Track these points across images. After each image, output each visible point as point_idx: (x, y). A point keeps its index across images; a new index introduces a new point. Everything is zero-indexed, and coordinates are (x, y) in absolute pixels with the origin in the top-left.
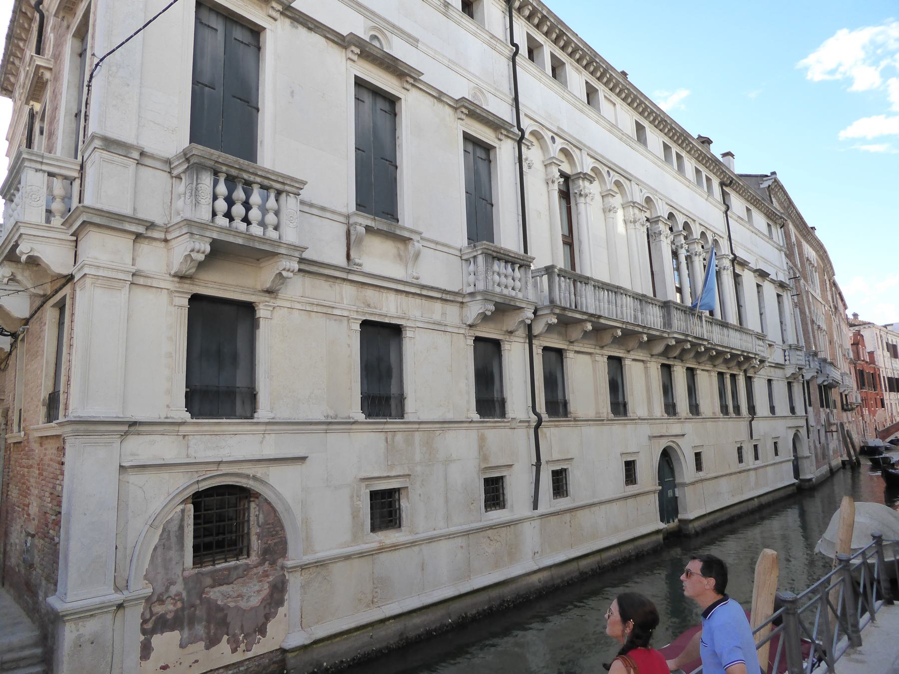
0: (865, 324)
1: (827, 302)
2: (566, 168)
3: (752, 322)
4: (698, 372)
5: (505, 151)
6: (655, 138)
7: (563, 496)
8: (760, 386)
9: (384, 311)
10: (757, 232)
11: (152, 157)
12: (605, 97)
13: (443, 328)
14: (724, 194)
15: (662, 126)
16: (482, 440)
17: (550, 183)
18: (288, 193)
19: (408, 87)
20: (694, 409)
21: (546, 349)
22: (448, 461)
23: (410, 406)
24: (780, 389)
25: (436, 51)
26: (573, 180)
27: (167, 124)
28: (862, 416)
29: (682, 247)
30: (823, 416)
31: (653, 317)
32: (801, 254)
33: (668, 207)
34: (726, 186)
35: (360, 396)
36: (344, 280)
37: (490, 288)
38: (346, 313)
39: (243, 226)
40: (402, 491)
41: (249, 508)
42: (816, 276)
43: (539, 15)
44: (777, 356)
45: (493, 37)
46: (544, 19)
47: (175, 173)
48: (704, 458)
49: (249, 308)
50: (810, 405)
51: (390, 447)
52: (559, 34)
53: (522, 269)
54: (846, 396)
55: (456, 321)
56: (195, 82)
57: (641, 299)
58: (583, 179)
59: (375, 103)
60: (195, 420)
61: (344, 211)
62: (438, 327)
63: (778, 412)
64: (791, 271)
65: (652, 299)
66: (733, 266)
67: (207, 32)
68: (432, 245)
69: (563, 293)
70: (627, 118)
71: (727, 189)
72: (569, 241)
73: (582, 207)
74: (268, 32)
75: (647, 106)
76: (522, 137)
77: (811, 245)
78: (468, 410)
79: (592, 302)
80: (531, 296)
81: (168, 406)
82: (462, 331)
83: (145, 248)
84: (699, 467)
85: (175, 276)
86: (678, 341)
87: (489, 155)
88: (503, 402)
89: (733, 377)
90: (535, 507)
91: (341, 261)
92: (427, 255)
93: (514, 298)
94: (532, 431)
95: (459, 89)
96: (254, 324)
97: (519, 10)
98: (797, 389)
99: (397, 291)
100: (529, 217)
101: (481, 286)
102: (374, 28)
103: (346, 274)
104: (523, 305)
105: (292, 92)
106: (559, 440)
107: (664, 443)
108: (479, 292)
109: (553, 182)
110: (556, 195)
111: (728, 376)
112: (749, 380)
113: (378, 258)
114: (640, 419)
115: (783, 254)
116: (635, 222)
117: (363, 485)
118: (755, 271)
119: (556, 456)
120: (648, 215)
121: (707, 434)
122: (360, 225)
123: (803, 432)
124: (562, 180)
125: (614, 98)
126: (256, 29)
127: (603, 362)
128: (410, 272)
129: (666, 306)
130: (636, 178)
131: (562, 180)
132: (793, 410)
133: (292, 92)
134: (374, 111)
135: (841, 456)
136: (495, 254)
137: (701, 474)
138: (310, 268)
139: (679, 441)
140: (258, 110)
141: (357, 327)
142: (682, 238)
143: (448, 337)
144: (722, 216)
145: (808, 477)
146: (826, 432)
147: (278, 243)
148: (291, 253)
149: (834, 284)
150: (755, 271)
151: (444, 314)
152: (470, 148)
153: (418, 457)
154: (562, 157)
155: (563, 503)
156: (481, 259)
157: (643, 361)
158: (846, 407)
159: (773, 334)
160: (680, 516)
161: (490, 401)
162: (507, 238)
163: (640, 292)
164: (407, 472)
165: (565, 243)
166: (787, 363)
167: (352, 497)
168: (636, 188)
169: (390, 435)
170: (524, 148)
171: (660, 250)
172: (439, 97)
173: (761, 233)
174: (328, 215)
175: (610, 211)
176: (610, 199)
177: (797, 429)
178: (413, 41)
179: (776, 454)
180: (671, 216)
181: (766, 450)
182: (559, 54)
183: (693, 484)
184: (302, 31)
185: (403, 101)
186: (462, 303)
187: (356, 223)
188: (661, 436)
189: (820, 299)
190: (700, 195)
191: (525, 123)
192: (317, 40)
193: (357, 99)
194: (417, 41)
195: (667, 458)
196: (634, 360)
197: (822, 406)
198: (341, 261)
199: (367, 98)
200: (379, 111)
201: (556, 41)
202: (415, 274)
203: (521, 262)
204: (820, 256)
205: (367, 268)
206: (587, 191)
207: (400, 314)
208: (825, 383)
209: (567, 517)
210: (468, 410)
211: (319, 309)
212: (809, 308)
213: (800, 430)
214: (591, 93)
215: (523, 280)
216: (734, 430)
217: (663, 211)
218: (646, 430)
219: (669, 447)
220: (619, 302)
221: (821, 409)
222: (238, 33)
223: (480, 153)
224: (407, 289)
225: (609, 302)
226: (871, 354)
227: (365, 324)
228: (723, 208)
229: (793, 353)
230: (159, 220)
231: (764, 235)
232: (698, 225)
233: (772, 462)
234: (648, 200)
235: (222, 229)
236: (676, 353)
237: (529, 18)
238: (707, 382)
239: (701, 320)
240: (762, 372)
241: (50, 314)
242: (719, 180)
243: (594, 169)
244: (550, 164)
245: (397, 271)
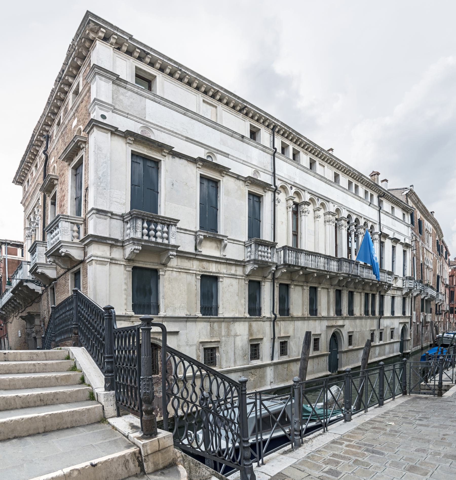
2: (297, 200)
3: (387, 267)
5: (268, 197)
6: (344, 180)
7: (284, 355)
8: (387, 300)
9: (210, 270)
11: (116, 215)
12: (320, 164)
13: (235, 277)
14: (380, 202)
15: (348, 173)
16: (250, 326)
17: (288, 208)
18: (172, 225)
19: (224, 175)
20: (351, 312)
21: (281, 284)
22: (236, 335)
23: (220, 311)
24: (398, 301)
25: (237, 158)
26: (300, 206)
27: (121, 202)
28: (449, 319)
29: (353, 231)
30: (422, 317)
31: (334, 266)
34: (381, 197)
35: (200, 306)
36: (194, 258)
37: (257, 258)
38: (195, 272)
39: (153, 239)
40: (217, 349)
41: (157, 353)
42: (431, 238)
44: (399, 284)
45: (264, 147)
47: (125, 220)
48: (353, 338)
49: (156, 271)
50: (414, 311)
51: (212, 328)
52: (298, 139)
53: (272, 249)
55: (241, 273)
56: (132, 185)
57: (328, 258)
58: (305, 204)
59: (209, 184)
60: (136, 315)
61: (194, 230)
62: (233, 276)
63: (396, 315)
64: (414, 237)
65: (335, 258)
66: (380, 238)
67: (136, 165)
68: (232, 242)
69: (291, 258)
70: (328, 172)
71: (382, 199)
72: (296, 234)
73: (303, 217)
74: (162, 162)
75: (341, 165)
76: (276, 189)
78: (245, 313)
79: (303, 261)
80: (275, 260)
81: (126, 310)
82: (244, 278)
83: (115, 249)
84: (350, 343)
85: (126, 259)
86: (344, 278)
87: (260, 200)
88: (260, 309)
89: (374, 296)
90: (272, 359)
91: (193, 251)
92: (229, 246)
93: (267, 262)
94: (272, 323)
95: (247, 172)
96: (157, 277)
97: (278, 132)
98: (408, 301)
99: (97, 257)
100: (277, 224)
101: (253, 257)
102: (208, 153)
103: (194, 256)
104: (271, 265)
105: (173, 184)
106: (284, 328)
107: (333, 330)
108: (252, 260)
109: (290, 208)
110: (290, 213)
111: (370, 295)
112: (382, 297)
113: (209, 249)
114: (323, 317)
115: (410, 229)
116: (329, 221)
117: (201, 345)
118: (392, 239)
119: (282, 335)
120: (337, 217)
121: (358, 327)
122: (201, 235)
124: (294, 206)
125: (324, 163)
126: (157, 161)
127: (307, 289)
128: (222, 253)
129: (340, 260)
131: (294, 206)
132: (404, 313)
133: (173, 184)
134: (208, 187)
135: (430, 342)
136: (259, 243)
137: (351, 347)
138: (182, 255)
139: (342, 329)
140: (158, 193)
141: (199, 277)
142: (354, 226)
143: (237, 280)
145: (407, 351)
146: (422, 326)
147: (168, 245)
148: (173, 248)
150: (392, 239)
151: (236, 271)
152: (251, 198)
153: (223, 333)
154: (295, 196)
155: (285, 358)
156: (253, 246)
158: (438, 313)
159: (398, 272)
160: (338, 370)
161: (254, 309)
162: (266, 235)
163: (328, 255)
164: (219, 340)
165: (294, 235)
166: (404, 287)
167: (197, 350)
168: (331, 205)
169: (212, 323)
170: (276, 195)
171: (341, 234)
172: (238, 177)
174: (188, 232)
175: (317, 217)
176: (318, 212)
177: (405, 324)
178: (227, 155)
180: (349, 216)
183: (346, 352)
184: (177, 159)
185: (221, 182)
186: (244, 265)
187: (200, 235)
188: (332, 326)
190: (366, 204)
191: (279, 184)
192: (184, 162)
193: (201, 183)
194: (229, 155)
195: (335, 338)
197: (422, 311)
198: (193, 251)
199: (206, 183)
200: (210, 187)
202: (224, 254)
203: (272, 245)
204: (434, 227)
205: (204, 253)
206: (306, 210)
207: (217, 271)
208: (426, 298)
209: (286, 366)
210: (245, 313)
211: (184, 271)
212: (423, 256)
213: (407, 325)
214: (312, 163)
215: (272, 254)
217: (345, 214)
218: (325, 323)
219: (336, 332)
220: (316, 260)
221: (421, 313)
222: (149, 164)
223: (256, 199)
224: (221, 261)
225: (312, 261)
227: (202, 276)
229: (408, 281)
230: (120, 239)
232: (363, 219)
234: (338, 210)
235: (146, 241)
236: (344, 284)
237: (283, 135)
238: (359, 300)
239: (358, 267)
240: (389, 292)
241: (70, 277)
242: (377, 195)
243: (310, 199)
244: (289, 199)
245: (216, 253)
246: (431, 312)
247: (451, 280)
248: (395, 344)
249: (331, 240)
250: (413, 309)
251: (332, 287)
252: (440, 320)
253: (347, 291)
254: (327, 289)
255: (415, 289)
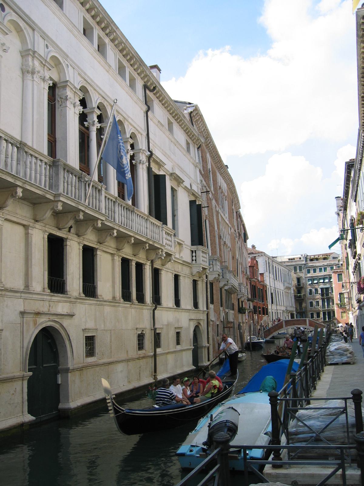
0: (259, 252)
1: (233, 226)
4: (99, 253)
10: (177, 143)
30: (223, 314)
32: (215, 181)
33: (80, 79)
42: (226, 203)
43: (151, 81)
46: (121, 43)
50: (212, 302)
54: (242, 302)
77: (224, 178)
123: (204, 326)
130: (40, 29)
139: (66, 323)
144: (142, 115)
146: (224, 328)
149: (239, 216)
157: (24, 226)
166: (194, 262)
173: (180, 144)
179: (178, 343)
181: (168, 339)
182: (102, 34)
183: (81, 369)
189: (228, 222)
196: (6, 220)
201: (103, 29)
208: (226, 288)
213: (202, 323)
216: (136, 317)
221: (221, 309)
226: (262, 275)
228: (145, 108)
231: (181, 146)
233: (172, 350)
240: (169, 265)
246: (233, 309)
247: (252, 271)
248: (184, 353)
249: (35, 117)
250: (209, 301)
251: (38, 225)
252: (244, 321)
253: (79, 243)
254: (25, 227)
255: (211, 270)
